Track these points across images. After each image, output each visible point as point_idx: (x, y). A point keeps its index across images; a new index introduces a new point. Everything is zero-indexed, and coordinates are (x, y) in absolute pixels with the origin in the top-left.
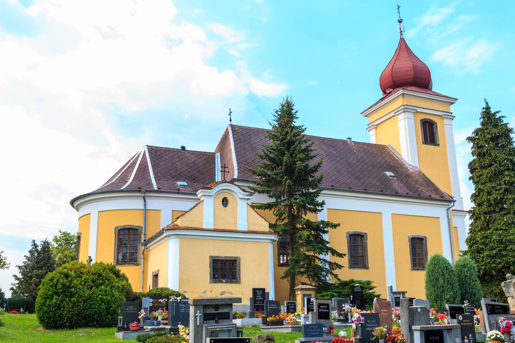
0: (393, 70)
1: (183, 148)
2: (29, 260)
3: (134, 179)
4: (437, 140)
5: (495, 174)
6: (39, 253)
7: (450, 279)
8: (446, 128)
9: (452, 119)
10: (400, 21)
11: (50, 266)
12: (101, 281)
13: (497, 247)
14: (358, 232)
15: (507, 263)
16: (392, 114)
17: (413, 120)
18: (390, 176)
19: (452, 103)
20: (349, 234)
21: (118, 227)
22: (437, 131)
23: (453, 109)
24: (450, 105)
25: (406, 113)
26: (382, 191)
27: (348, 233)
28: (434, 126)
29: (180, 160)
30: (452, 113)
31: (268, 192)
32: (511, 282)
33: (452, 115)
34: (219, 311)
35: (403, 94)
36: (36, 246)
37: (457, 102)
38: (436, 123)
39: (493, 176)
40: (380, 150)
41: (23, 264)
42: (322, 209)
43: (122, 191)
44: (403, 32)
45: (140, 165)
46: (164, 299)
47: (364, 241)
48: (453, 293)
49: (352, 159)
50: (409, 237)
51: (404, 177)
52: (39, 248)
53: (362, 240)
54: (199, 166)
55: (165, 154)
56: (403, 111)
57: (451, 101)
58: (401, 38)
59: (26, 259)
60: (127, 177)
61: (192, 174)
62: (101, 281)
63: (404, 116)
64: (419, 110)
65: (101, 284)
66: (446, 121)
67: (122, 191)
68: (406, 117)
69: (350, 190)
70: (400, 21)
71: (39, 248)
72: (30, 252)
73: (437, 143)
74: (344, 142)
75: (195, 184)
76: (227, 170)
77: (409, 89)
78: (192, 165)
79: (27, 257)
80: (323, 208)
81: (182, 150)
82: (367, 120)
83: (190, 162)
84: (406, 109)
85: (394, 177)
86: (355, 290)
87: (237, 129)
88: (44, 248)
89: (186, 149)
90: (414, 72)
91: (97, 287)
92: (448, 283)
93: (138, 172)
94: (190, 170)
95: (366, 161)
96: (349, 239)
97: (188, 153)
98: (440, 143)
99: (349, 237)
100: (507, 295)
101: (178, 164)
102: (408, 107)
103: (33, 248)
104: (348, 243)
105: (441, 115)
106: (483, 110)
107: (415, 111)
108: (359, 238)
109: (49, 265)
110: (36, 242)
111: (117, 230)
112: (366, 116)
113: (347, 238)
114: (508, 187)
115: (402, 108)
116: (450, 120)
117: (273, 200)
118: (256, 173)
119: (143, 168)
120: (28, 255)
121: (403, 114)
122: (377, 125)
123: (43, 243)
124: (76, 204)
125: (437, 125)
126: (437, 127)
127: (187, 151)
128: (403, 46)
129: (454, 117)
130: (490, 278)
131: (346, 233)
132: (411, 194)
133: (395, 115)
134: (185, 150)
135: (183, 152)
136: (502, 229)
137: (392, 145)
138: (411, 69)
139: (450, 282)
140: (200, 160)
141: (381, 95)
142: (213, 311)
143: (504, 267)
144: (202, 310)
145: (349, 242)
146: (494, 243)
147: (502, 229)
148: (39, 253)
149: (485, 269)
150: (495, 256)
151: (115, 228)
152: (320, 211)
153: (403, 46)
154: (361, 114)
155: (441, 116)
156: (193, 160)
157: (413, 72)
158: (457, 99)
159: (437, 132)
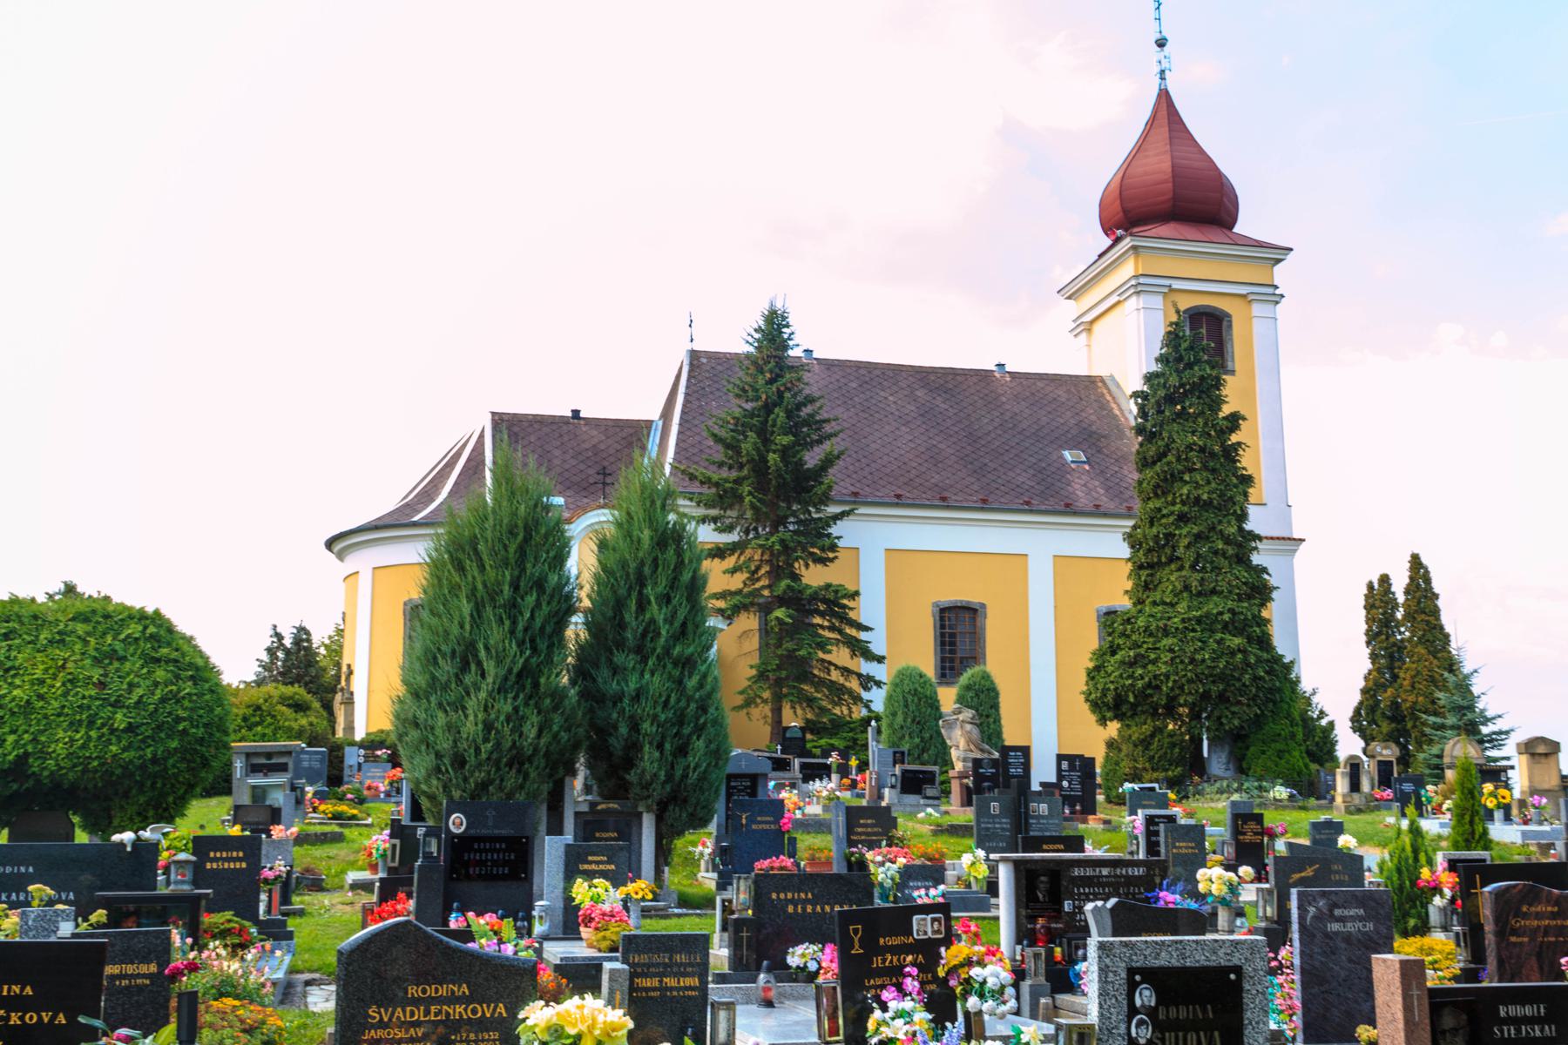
0: (1125, 182)
1: (576, 413)
2: (264, 667)
3: (451, 493)
4: (1229, 359)
5: (1166, 480)
6: (287, 652)
7: (917, 714)
8: (1258, 327)
9: (1277, 303)
10: (1161, 43)
11: (311, 682)
12: (258, 719)
13: (1144, 642)
14: (961, 601)
15: (1155, 677)
16: (1114, 299)
17: (1162, 312)
18: (1072, 462)
19: (1279, 261)
20: (938, 606)
21: (410, 600)
22: (1231, 335)
23: (1280, 274)
24: (1274, 265)
25: (1142, 297)
26: (1027, 503)
27: (935, 604)
28: (1225, 324)
29: (562, 444)
30: (1276, 287)
31: (715, 520)
32: (957, 719)
33: (1277, 292)
34: (273, 761)
35: (1134, 248)
36: (279, 636)
37: (1291, 257)
38: (1229, 316)
39: (1161, 484)
40: (1079, 392)
41: (254, 678)
42: (836, 557)
43: (415, 525)
44: (1167, 72)
45: (469, 460)
46: (384, 750)
47: (978, 624)
48: (922, 741)
49: (986, 421)
50: (1098, 611)
51: (1113, 461)
52: (288, 642)
53: (974, 619)
54: (604, 455)
55: (530, 430)
56: (1132, 291)
57: (1276, 254)
58: (1160, 90)
59: (259, 666)
60: (438, 489)
61: (584, 477)
62: (258, 719)
63: (1138, 301)
64: (1177, 285)
65: (257, 724)
66: (1257, 309)
67: (415, 525)
68: (1141, 305)
69: (944, 503)
70: (1161, 43)
71: (288, 642)
72: (269, 650)
73: (1230, 368)
74: (983, 376)
75: (585, 500)
76: (609, 480)
77: (1153, 232)
78: (590, 454)
79: (262, 661)
80: (837, 554)
81: (573, 418)
82: (1073, 309)
83: (586, 445)
84: (1139, 287)
85: (1084, 462)
86: (788, 735)
87: (704, 361)
88: (297, 641)
89: (582, 415)
90: (1174, 186)
91: (250, 729)
92: (913, 721)
93: (462, 477)
94: (582, 467)
95: (1025, 424)
96: (938, 618)
97: (585, 425)
98: (1237, 367)
99: (938, 614)
100: (948, 742)
101: (557, 453)
102: (1142, 280)
103: (273, 642)
104: (935, 627)
105: (1244, 292)
106: (1169, 329)
107: (1166, 290)
108: (967, 615)
109: (307, 679)
110: (278, 630)
111: (409, 607)
112: (1069, 298)
113: (934, 616)
114: (1186, 509)
115: (1133, 282)
116: (1271, 306)
117: (733, 537)
118: (696, 477)
119: (475, 465)
120: (265, 657)
121: (1134, 298)
122: (1092, 322)
123: (295, 631)
124: (338, 547)
125: (1230, 322)
126: (1230, 326)
127: (584, 419)
128: (1166, 112)
129: (1282, 296)
130: (632, 717)
131: (930, 605)
132: (1109, 505)
133: (1118, 303)
134: (580, 418)
135: (573, 424)
136: (1164, 603)
137: (1116, 377)
138: (1166, 177)
139: (918, 719)
140: (610, 441)
141: (1108, 242)
142: (263, 761)
143: (1149, 685)
144: (244, 759)
145: (938, 626)
146: (1140, 634)
147: (1164, 603)
148: (287, 652)
149: (1116, 689)
150: (1135, 663)
151: (405, 604)
152: (832, 560)
153: (1166, 112)
154: (1058, 292)
155: (1244, 296)
156: (595, 441)
157: (1170, 185)
158: (1291, 250)
159: (1231, 340)
